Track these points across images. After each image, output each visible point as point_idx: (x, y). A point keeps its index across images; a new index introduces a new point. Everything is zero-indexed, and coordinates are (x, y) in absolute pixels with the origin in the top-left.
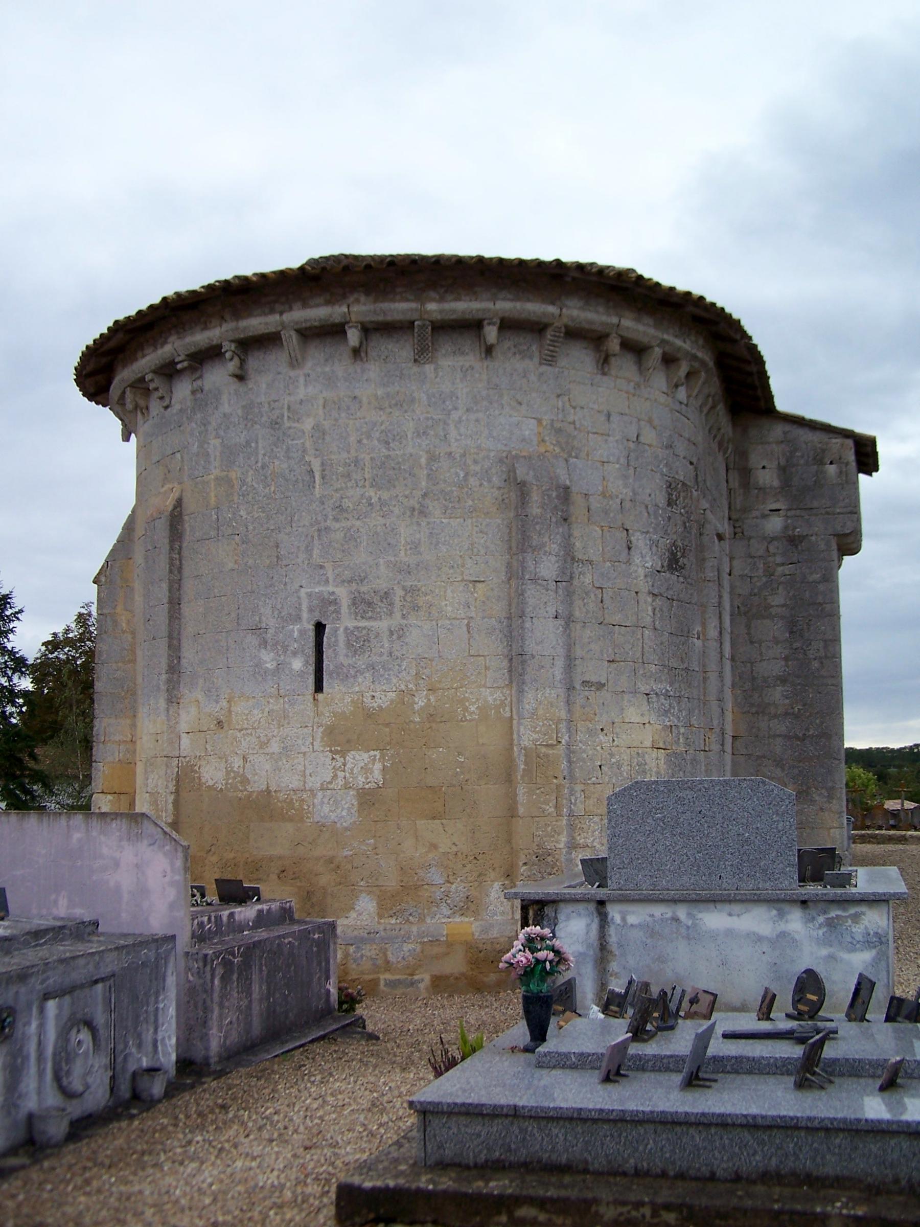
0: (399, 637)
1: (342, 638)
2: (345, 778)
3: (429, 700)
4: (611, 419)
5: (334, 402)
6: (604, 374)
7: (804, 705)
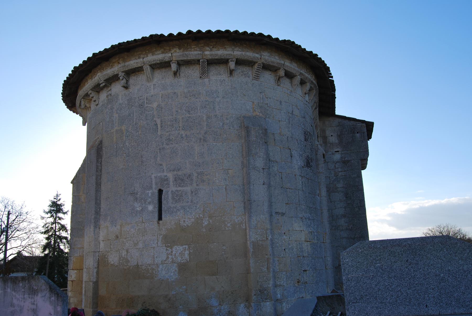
0: (196, 194)
2: (172, 258)
3: (209, 221)
6: (278, 85)
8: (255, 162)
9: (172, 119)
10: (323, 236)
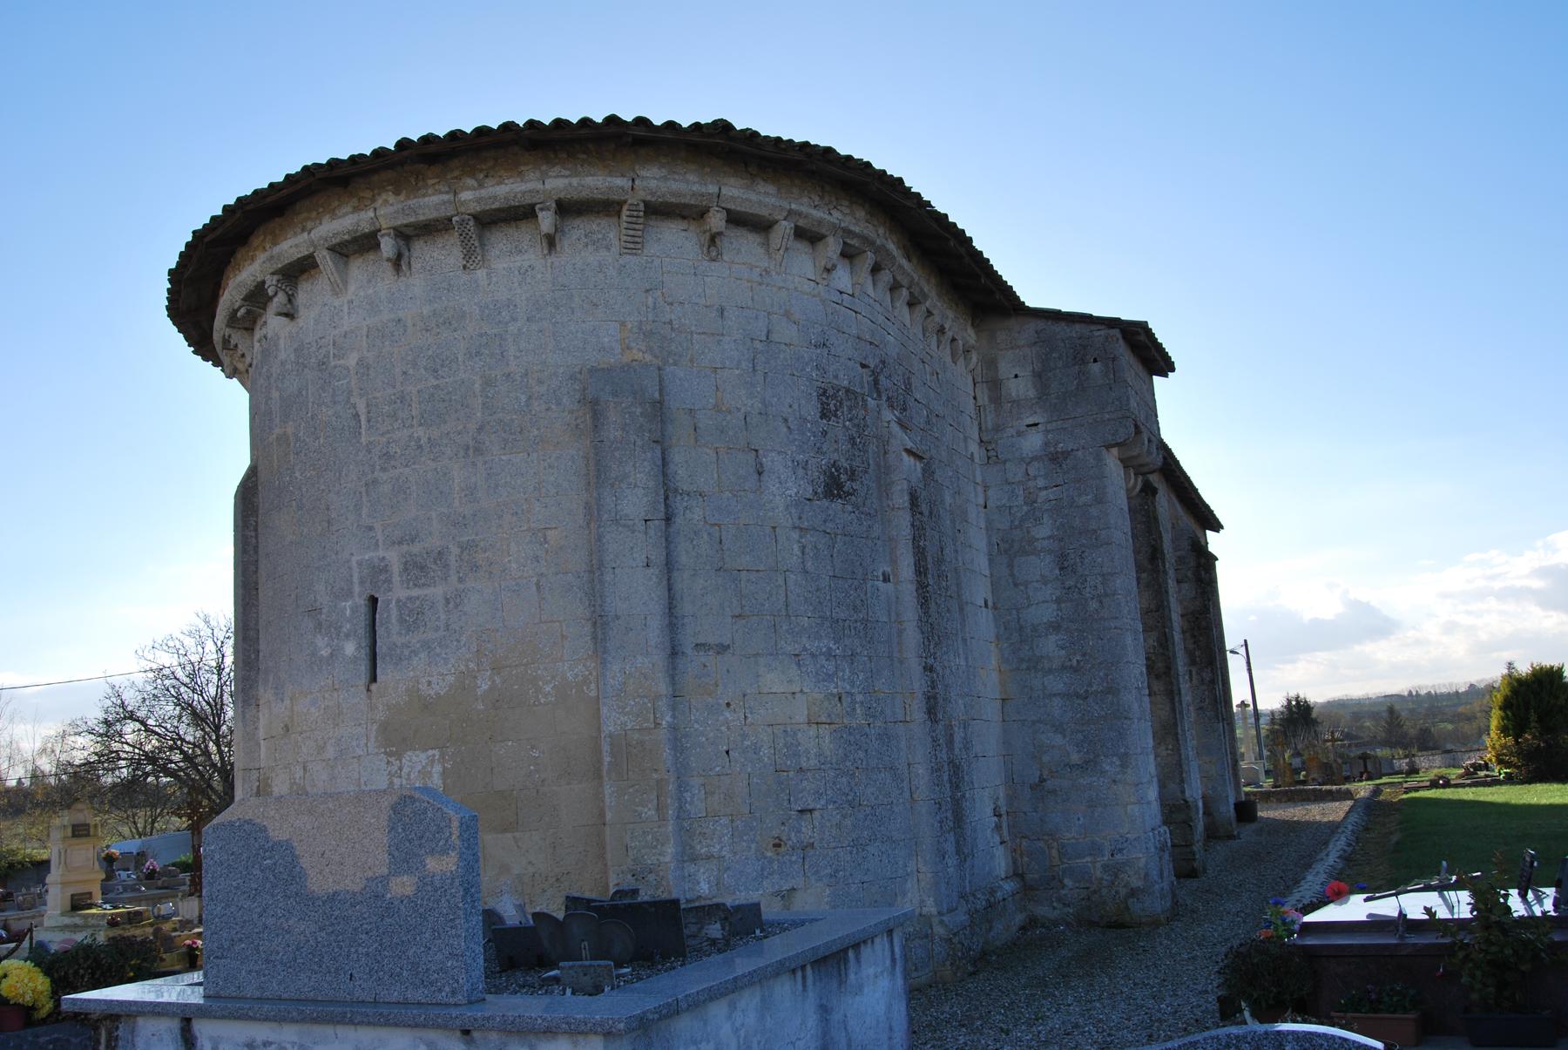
0: (457, 606)
1: (394, 613)
3: (494, 681)
4: (726, 313)
5: (378, 330)
7: (1084, 655)
8: (619, 502)
9: (393, 397)
10: (905, 703)
